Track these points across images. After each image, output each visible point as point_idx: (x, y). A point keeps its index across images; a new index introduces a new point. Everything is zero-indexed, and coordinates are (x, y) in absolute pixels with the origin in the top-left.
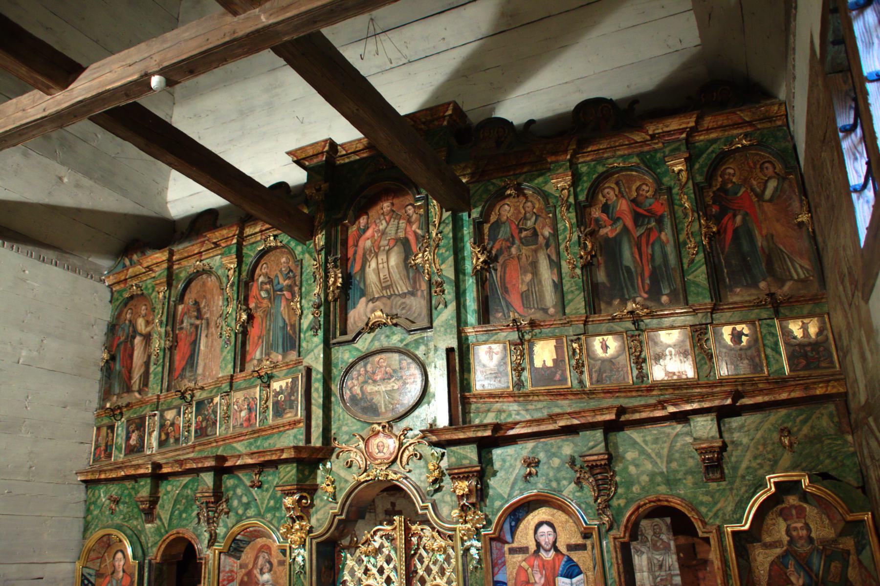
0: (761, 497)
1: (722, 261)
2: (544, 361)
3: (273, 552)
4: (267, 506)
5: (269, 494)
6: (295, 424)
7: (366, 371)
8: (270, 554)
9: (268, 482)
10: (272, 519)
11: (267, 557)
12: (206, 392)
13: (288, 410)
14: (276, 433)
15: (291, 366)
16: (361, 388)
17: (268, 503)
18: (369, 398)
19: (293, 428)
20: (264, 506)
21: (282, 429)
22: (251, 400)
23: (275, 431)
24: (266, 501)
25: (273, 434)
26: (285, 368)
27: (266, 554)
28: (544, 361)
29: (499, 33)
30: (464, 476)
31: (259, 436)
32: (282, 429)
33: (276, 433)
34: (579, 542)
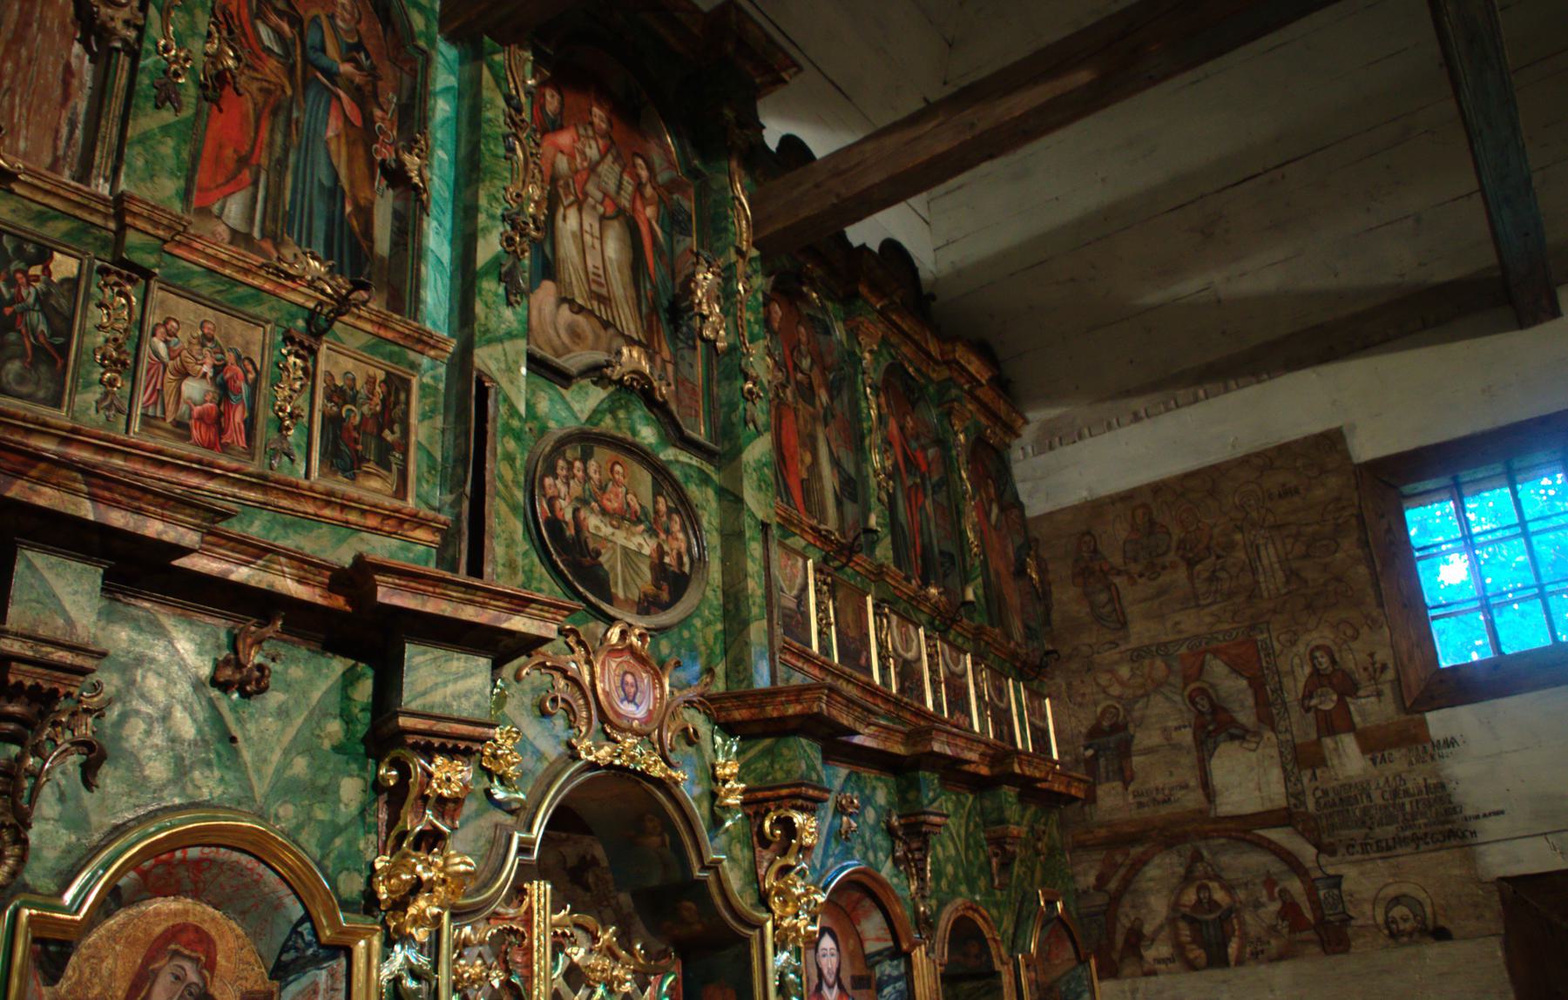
0: (1307, 852)
1: (970, 535)
2: (221, 110)
3: (220, 959)
4: (278, 771)
5: (291, 732)
6: (402, 522)
7: (587, 478)
8: (211, 965)
9: (288, 686)
10: (300, 827)
11: (193, 977)
12: (13, 204)
13: (370, 466)
14: (330, 522)
15: (390, 335)
16: (576, 511)
17: (286, 764)
18: (591, 545)
19: (389, 534)
20: (270, 770)
21: (353, 517)
22: (230, 357)
23: (327, 512)
24: (276, 757)
25: (318, 519)
26: (368, 327)
27: (188, 965)
28: (221, 110)
29: (833, 83)
30: (443, 746)
31: (263, 506)
32: (353, 517)
33: (330, 522)
34: (864, 973)
